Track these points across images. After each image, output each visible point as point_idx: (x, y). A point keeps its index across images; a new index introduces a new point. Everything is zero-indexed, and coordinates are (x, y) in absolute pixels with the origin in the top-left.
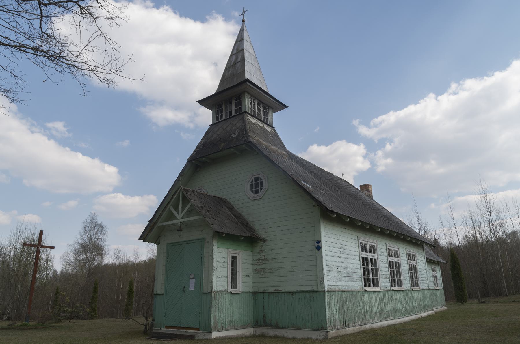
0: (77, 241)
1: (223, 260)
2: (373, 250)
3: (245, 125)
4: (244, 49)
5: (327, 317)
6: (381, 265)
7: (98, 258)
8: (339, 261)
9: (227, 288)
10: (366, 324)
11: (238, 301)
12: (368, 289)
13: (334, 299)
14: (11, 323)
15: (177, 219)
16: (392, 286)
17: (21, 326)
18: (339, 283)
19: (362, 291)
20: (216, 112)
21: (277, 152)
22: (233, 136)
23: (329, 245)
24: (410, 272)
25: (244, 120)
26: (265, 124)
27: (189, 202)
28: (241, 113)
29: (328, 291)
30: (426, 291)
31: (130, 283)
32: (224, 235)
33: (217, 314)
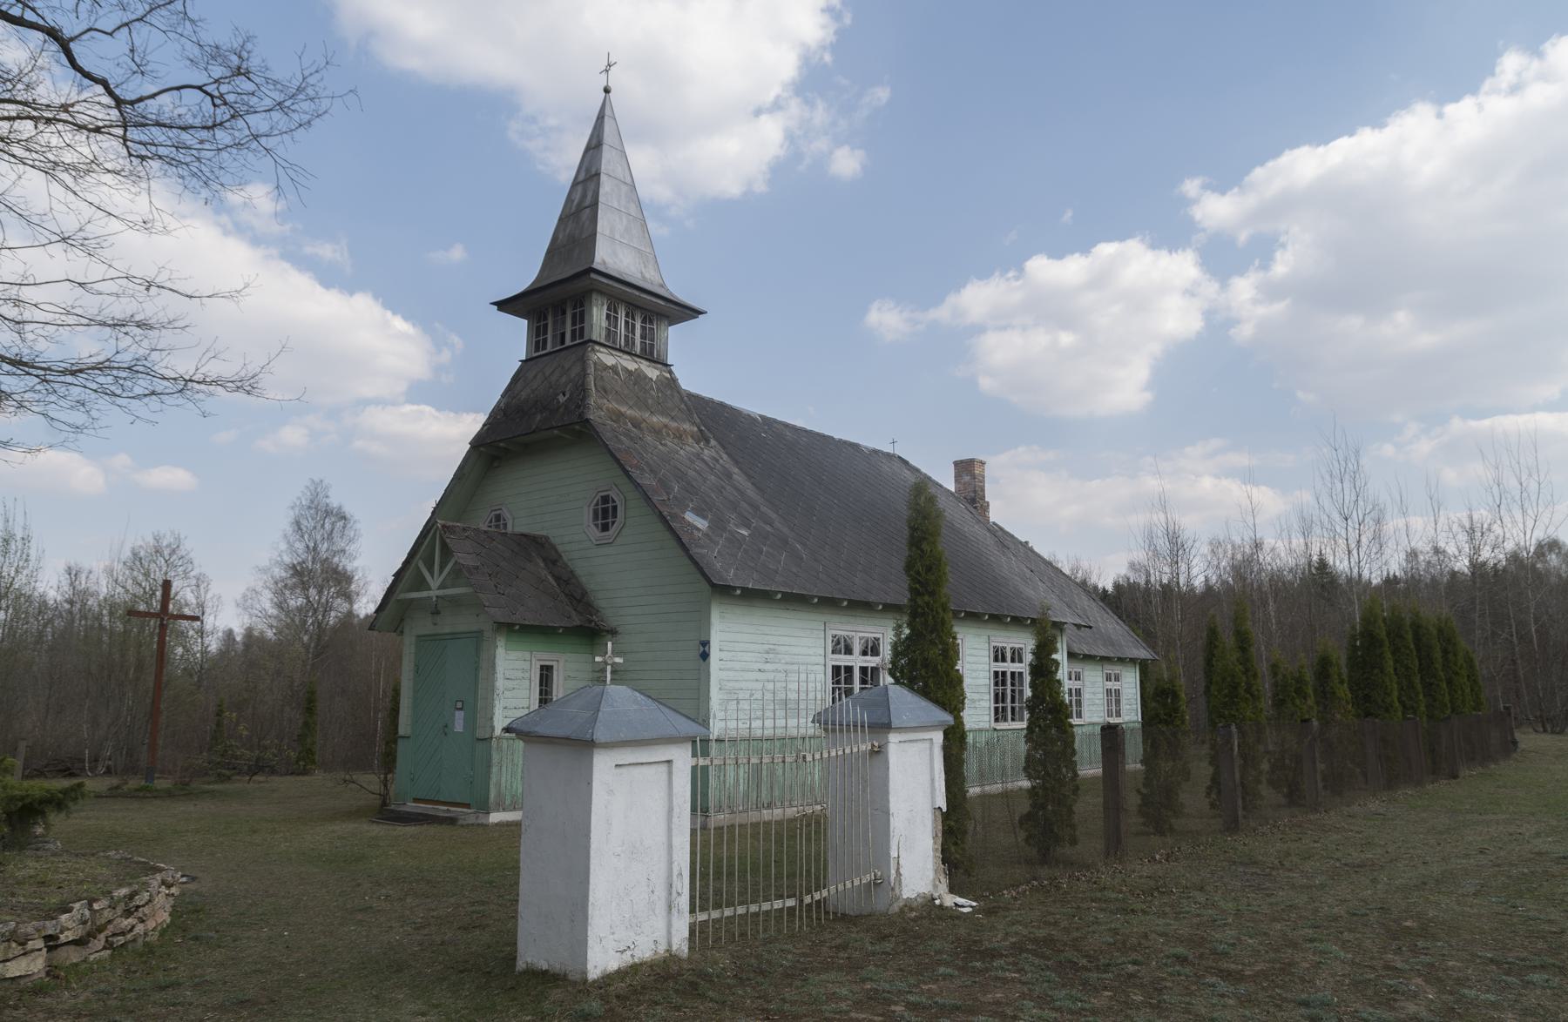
0: (279, 559)
1: (520, 674)
7: (341, 605)
14: (115, 781)
15: (430, 589)
17: (137, 790)
20: (535, 329)
28: (584, 343)
31: (393, 690)
33: (503, 780)
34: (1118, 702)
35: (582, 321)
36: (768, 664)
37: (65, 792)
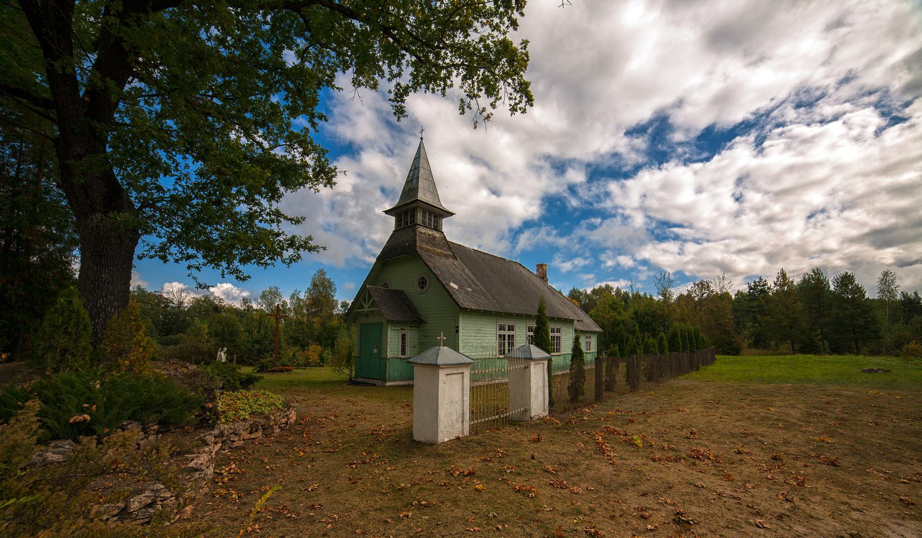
28: (414, 225)
34: (590, 345)
35: (414, 217)
37: (259, 377)
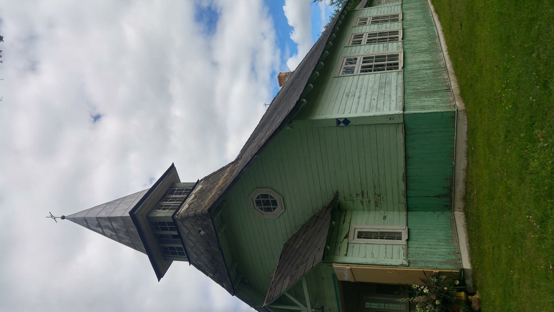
2: (352, 61)
3: (189, 217)
4: (96, 217)
5: (438, 111)
6: (371, 52)
8: (364, 97)
9: (400, 246)
10: (446, 66)
11: (418, 230)
12: (401, 65)
13: (414, 103)
16: (398, 40)
18: (394, 98)
19: (404, 71)
21: (227, 178)
22: (202, 233)
23: (343, 110)
24: (381, 23)
25: (185, 218)
26: (192, 193)
27: (284, 295)
28: (174, 223)
29: (404, 109)
30: (403, 7)
32: (328, 247)
33: (437, 260)
35: (164, 223)
36: (355, 95)
